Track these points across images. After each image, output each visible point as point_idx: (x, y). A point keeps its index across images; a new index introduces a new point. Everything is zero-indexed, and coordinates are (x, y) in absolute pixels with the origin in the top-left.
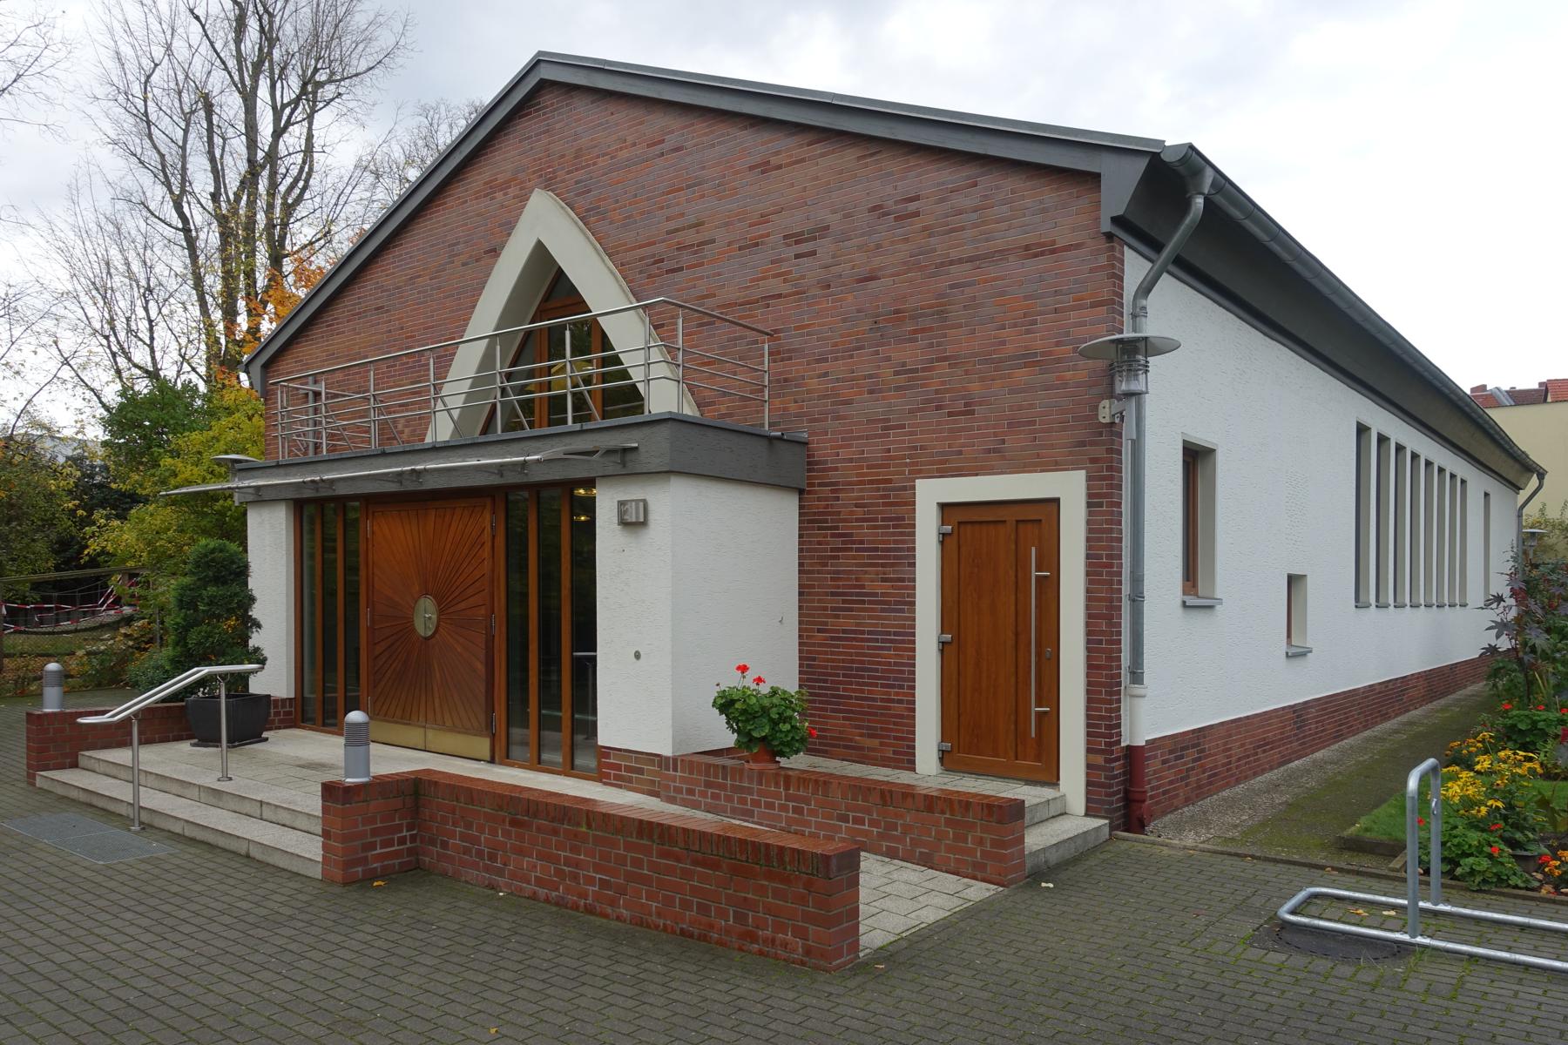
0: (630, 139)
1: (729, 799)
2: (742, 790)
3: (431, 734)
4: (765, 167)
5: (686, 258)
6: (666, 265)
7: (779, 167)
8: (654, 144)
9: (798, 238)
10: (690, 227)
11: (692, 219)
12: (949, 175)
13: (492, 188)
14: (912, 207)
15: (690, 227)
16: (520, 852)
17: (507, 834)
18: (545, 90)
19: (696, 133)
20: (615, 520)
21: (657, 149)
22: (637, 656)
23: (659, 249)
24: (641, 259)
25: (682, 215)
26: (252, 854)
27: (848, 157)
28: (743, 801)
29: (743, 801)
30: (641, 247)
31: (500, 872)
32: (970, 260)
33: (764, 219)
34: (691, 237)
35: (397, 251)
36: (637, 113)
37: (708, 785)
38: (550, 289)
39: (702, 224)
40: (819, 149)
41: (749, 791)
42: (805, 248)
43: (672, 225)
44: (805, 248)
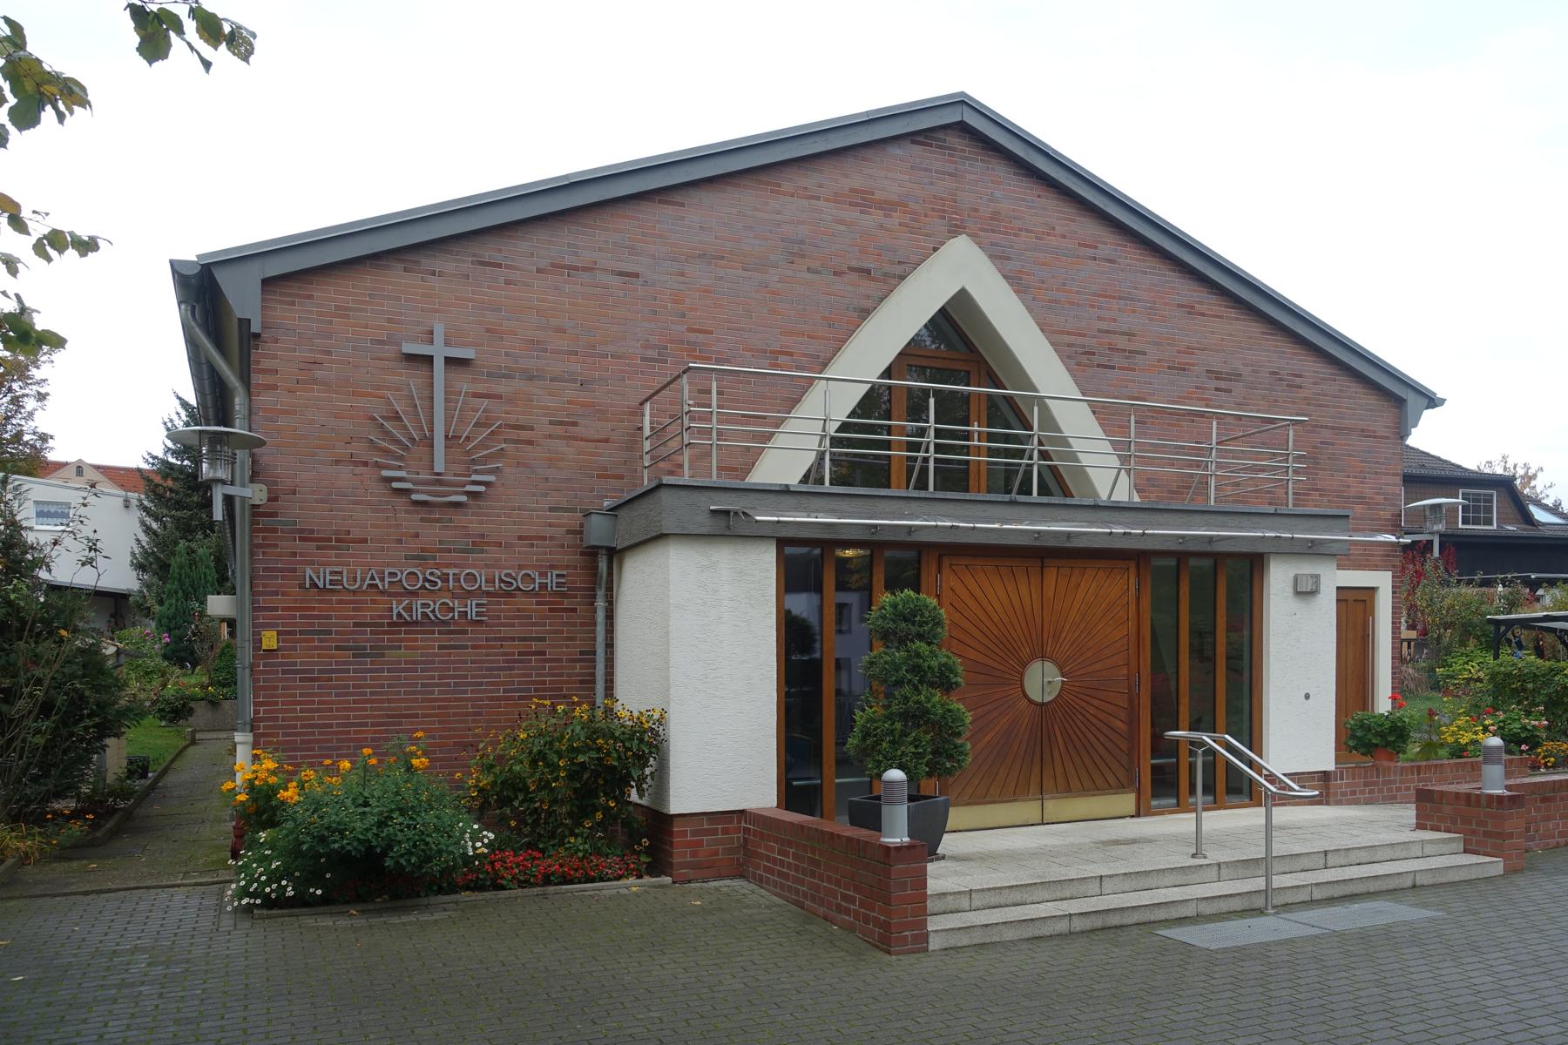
0: (1059, 229)
1: (1381, 791)
2: (1390, 782)
3: (1050, 805)
4: (1190, 310)
5: (1117, 360)
6: (1097, 359)
7: (1203, 314)
8: (1085, 246)
9: (1218, 376)
10: (1123, 334)
11: (1125, 328)
12: (1324, 370)
13: (863, 200)
14: (1298, 381)
15: (1123, 334)
16: (1548, 819)
17: (1538, 809)
18: (961, 134)
19: (1130, 256)
20: (1290, 590)
21: (1090, 252)
22: (1307, 697)
23: (1091, 342)
24: (1070, 345)
25: (1115, 320)
26: (1418, 883)
27: (1256, 328)
28: (1390, 790)
29: (1390, 790)
30: (1068, 333)
31: (1532, 839)
32: (1333, 428)
33: (1190, 350)
34: (1122, 342)
35: (669, 210)
36: (1069, 210)
37: (1366, 785)
38: (955, 339)
39: (1134, 335)
40: (1233, 313)
41: (1394, 782)
42: (1223, 384)
43: (1104, 325)
44: (1223, 384)
